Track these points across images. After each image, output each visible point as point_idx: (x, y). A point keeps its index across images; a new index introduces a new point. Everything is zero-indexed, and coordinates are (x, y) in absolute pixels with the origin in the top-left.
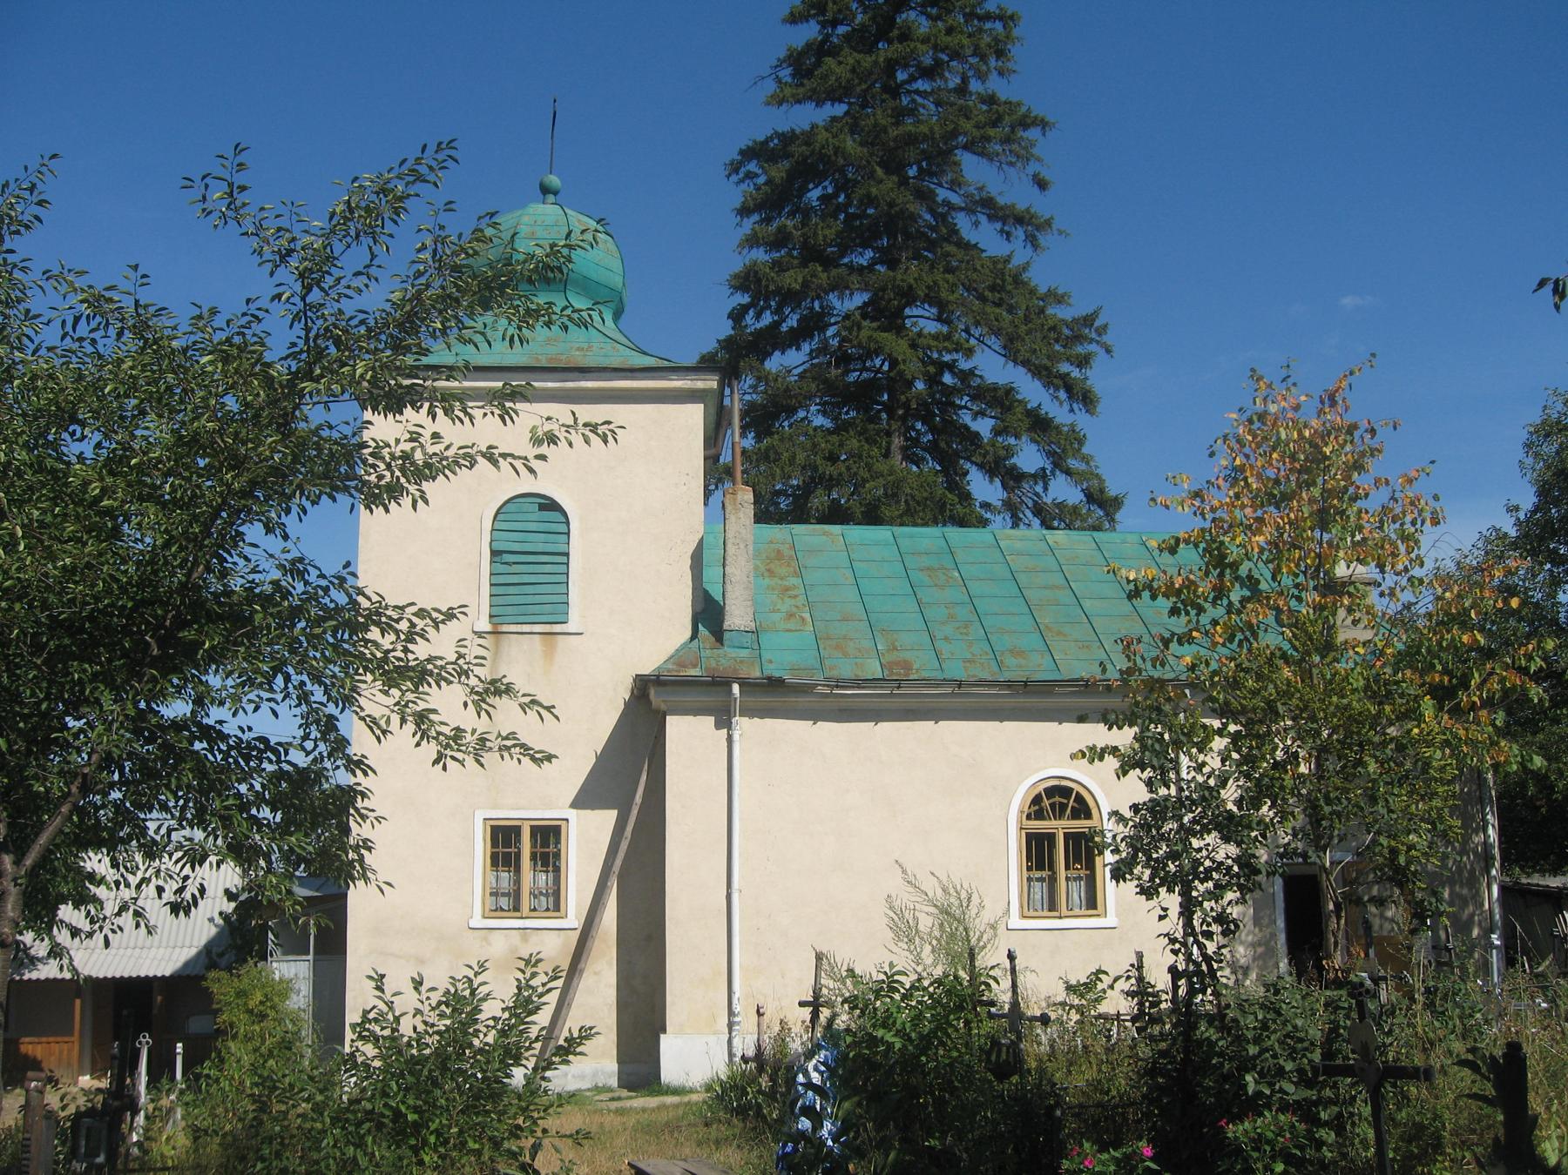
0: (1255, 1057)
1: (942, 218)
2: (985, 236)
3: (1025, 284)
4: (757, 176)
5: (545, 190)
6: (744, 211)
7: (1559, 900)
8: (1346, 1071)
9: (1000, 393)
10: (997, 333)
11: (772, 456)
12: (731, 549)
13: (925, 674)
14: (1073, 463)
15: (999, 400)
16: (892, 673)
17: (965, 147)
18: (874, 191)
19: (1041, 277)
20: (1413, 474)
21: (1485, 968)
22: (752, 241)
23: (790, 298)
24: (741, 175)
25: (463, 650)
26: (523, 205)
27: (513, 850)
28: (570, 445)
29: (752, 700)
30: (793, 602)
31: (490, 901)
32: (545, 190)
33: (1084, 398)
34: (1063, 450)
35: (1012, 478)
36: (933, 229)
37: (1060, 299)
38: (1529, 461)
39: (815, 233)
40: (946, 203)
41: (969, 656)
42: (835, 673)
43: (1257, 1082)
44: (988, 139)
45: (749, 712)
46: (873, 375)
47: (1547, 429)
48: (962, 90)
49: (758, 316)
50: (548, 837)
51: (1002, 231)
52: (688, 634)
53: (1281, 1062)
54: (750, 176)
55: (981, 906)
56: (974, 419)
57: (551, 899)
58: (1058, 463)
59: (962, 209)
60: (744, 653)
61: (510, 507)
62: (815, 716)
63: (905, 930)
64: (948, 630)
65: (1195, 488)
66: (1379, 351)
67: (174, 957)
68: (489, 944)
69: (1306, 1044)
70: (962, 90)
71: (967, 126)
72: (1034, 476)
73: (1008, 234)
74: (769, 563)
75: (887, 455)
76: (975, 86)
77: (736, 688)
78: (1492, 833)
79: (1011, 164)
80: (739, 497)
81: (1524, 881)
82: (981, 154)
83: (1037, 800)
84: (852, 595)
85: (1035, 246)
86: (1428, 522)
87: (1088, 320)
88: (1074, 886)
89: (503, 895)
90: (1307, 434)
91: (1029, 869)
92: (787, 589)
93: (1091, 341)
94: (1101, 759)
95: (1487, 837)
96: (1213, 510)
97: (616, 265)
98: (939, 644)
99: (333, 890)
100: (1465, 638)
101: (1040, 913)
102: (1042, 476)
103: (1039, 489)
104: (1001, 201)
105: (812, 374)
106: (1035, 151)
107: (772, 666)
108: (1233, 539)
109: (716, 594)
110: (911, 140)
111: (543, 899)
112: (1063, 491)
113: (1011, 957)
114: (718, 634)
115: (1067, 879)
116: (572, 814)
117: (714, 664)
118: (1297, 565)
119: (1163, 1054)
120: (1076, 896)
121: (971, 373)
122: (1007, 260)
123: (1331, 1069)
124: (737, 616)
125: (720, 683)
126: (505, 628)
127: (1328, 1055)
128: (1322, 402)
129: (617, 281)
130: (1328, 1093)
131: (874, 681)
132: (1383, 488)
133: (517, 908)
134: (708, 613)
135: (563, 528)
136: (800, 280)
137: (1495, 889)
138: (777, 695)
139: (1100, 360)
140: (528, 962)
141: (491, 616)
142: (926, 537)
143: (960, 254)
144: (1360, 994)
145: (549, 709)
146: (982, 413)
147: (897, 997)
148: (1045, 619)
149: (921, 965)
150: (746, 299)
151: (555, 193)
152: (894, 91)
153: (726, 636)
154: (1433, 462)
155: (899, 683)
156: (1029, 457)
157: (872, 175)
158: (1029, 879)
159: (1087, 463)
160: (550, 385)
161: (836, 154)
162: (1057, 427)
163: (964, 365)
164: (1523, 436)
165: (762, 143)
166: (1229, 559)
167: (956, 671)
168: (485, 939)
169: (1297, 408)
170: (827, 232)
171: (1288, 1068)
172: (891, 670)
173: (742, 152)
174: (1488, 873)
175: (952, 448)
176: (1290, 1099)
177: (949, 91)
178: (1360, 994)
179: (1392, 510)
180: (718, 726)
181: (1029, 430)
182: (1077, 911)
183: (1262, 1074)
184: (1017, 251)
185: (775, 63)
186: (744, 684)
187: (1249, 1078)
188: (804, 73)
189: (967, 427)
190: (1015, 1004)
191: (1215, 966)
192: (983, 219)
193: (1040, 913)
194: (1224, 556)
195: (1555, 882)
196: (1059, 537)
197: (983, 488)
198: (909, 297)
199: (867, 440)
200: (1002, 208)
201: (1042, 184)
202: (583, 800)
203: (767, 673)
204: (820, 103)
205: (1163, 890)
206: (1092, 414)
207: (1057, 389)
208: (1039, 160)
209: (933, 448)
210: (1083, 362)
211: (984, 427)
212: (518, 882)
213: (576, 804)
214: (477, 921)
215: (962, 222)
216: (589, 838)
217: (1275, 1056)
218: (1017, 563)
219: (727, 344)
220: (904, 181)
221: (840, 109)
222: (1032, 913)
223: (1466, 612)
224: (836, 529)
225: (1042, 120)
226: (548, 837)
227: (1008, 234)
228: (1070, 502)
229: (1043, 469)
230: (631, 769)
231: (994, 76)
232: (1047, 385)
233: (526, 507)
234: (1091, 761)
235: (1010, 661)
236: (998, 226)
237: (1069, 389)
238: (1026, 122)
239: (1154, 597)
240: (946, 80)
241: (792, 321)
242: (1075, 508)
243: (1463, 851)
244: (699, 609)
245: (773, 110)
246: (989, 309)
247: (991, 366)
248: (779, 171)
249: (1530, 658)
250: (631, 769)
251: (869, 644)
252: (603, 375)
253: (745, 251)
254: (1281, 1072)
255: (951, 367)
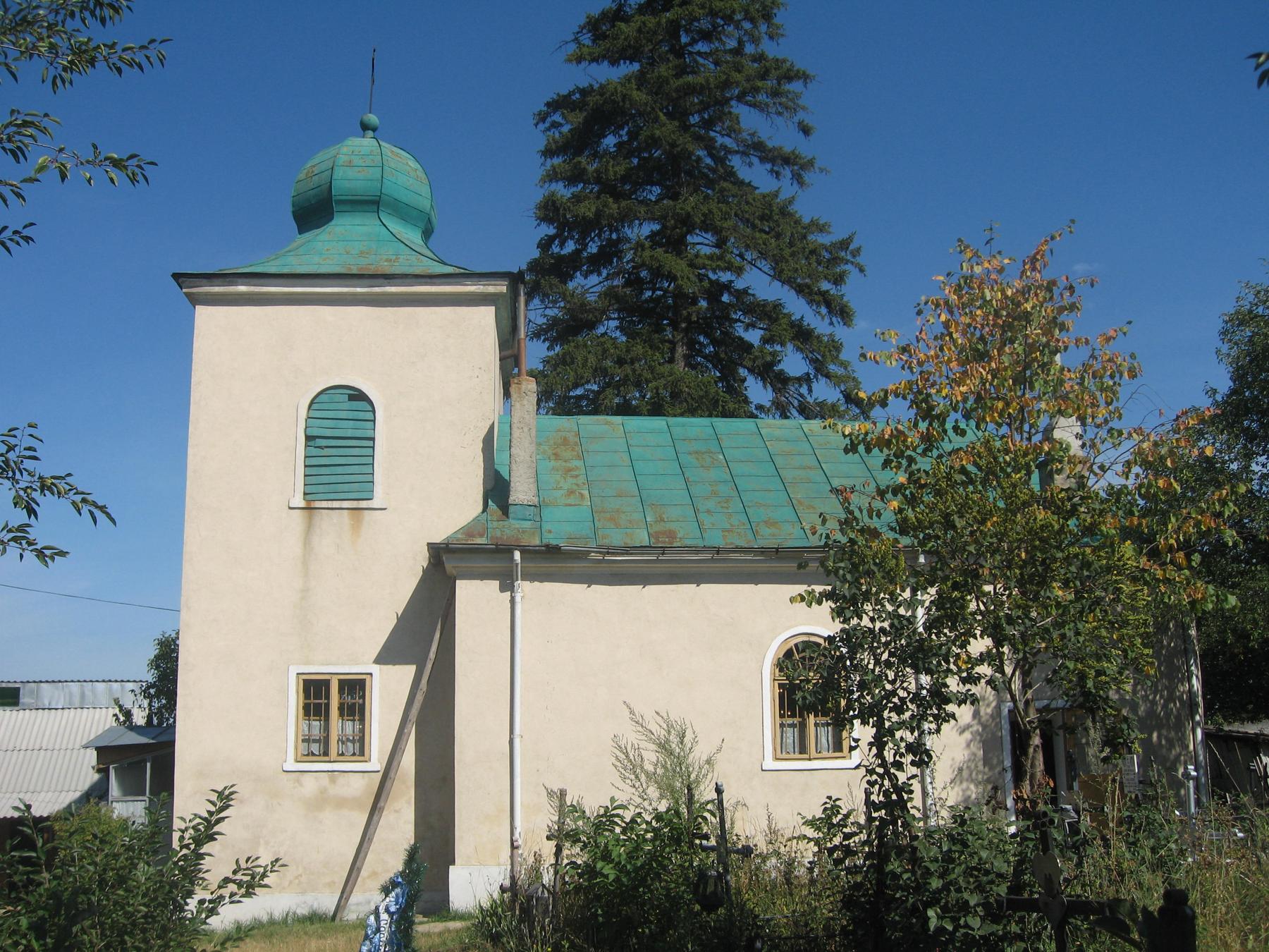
0: (939, 891)
1: (720, 161)
2: (756, 175)
3: (791, 215)
4: (561, 125)
5: (365, 127)
6: (548, 153)
7: (1256, 745)
8: (1031, 906)
9: (768, 309)
10: (763, 255)
11: (568, 360)
12: (516, 433)
13: (688, 542)
14: (832, 368)
15: (768, 313)
16: (658, 542)
17: (740, 98)
18: (657, 132)
19: (805, 209)
20: (1112, 333)
21: (1182, 804)
22: (552, 176)
23: (585, 227)
24: (547, 125)
25: (12, 441)
26: (339, 139)
27: (323, 701)
28: (63, 177)
29: (532, 566)
30: (574, 481)
31: (303, 747)
32: (365, 127)
33: (843, 313)
34: (823, 356)
35: (780, 381)
36: (714, 171)
37: (821, 229)
38: (1225, 349)
39: (607, 170)
40: (724, 147)
41: (728, 526)
42: (606, 542)
43: (939, 917)
44: (757, 90)
45: (530, 577)
46: (650, 281)
47: (1241, 319)
48: (738, 51)
49: (562, 245)
50: (355, 688)
51: (772, 171)
52: (480, 509)
53: (966, 895)
54: (555, 125)
55: (695, 741)
56: (746, 329)
57: (357, 745)
58: (820, 368)
59: (737, 152)
60: (527, 524)
61: (323, 398)
62: (590, 579)
63: (630, 765)
64: (710, 505)
65: (903, 344)
66: (1094, 268)
67: (60, 801)
68: (301, 785)
69: (992, 876)
70: (738, 51)
71: (737, 76)
72: (799, 380)
73: (778, 174)
74: (556, 450)
75: (671, 360)
76: (749, 49)
77: (517, 555)
78: (1196, 684)
79: (780, 114)
80: (523, 387)
81: (1226, 728)
82: (753, 105)
83: (789, 654)
84: (627, 474)
85: (801, 183)
86: (1126, 374)
87: (844, 244)
88: (822, 731)
89: (315, 741)
90: (1009, 293)
91: (782, 716)
92: (570, 470)
93: (847, 262)
94: (820, 603)
95: (1191, 686)
96: (920, 364)
97: (425, 190)
98: (702, 516)
99: (163, 738)
100: (1161, 483)
101: (792, 756)
102: (806, 379)
103: (804, 390)
104: (770, 144)
105: (610, 294)
106: (800, 102)
107: (551, 536)
108: (939, 391)
109: (504, 473)
110: (691, 90)
111: (350, 745)
112: (824, 391)
113: (719, 790)
114: (505, 508)
115: (816, 725)
116: (376, 669)
117: (498, 534)
118: (1001, 416)
119: (857, 886)
120: (824, 740)
121: (745, 291)
122: (776, 195)
123: (1016, 903)
124: (522, 491)
125: (502, 550)
126: (318, 504)
127: (1016, 888)
128: (1025, 264)
129: (425, 203)
130: (1014, 928)
131: (642, 549)
132: (1083, 348)
133: (326, 753)
134: (497, 490)
135: (369, 416)
136: (593, 209)
137: (1199, 732)
138: (554, 561)
139: (853, 276)
140: (220, 794)
141: (305, 494)
142: (697, 426)
143: (734, 190)
144: (1044, 824)
145: (102, 509)
146: (753, 325)
147: (618, 830)
148: (798, 494)
149: (644, 802)
150: (551, 231)
151: (374, 130)
152: (679, 52)
153: (511, 509)
154: (1130, 323)
155: (663, 550)
156: (793, 363)
157: (656, 119)
158: (782, 725)
159: (846, 368)
160: (359, 290)
161: (623, 101)
162: (818, 337)
163: (740, 284)
164: (1220, 325)
165: (565, 97)
166: (937, 411)
167: (716, 539)
168: (298, 781)
169: (1001, 270)
170: (617, 169)
171: (972, 903)
172: (657, 539)
173: (548, 104)
174: (1193, 719)
175: (730, 358)
176: (977, 934)
177: (725, 52)
178: (1044, 824)
179: (1091, 366)
180: (502, 589)
181: (793, 339)
182: (825, 754)
183: (945, 909)
184: (786, 188)
185: (577, 29)
186: (524, 552)
187: (931, 913)
188: (602, 35)
189: (741, 339)
190: (722, 837)
191: (905, 796)
192: (755, 160)
193: (792, 756)
194: (931, 408)
195: (1252, 729)
196: (815, 425)
197: (757, 391)
198: (687, 224)
199: (651, 347)
200: (770, 151)
201: (806, 130)
202: (386, 657)
203: (545, 541)
204: (614, 62)
205: (857, 722)
206: (849, 326)
207: (818, 304)
208: (803, 108)
209: (715, 359)
210: (839, 280)
211: (754, 337)
212: (327, 728)
213: (380, 660)
214: (291, 765)
215: (735, 161)
216: (390, 691)
217: (959, 890)
218: (774, 447)
219: (534, 266)
220: (685, 127)
221: (636, 67)
222: (784, 755)
223: (1162, 459)
224: (618, 419)
225: (804, 73)
226: (355, 688)
227: (778, 174)
228: (829, 401)
229: (808, 374)
230: (425, 630)
231: (765, 39)
232: (810, 302)
233: (337, 398)
234: (810, 605)
235: (765, 531)
236: (769, 166)
237: (828, 304)
238: (791, 75)
239: (868, 450)
240: (724, 44)
241: (593, 248)
242: (834, 407)
243: (1171, 698)
244: (489, 487)
245: (573, 67)
246: (758, 235)
247: (759, 283)
248: (578, 118)
249: (1224, 503)
250: (425, 630)
251: (638, 516)
252: (408, 281)
253: (547, 185)
254: (965, 907)
255: (727, 287)
